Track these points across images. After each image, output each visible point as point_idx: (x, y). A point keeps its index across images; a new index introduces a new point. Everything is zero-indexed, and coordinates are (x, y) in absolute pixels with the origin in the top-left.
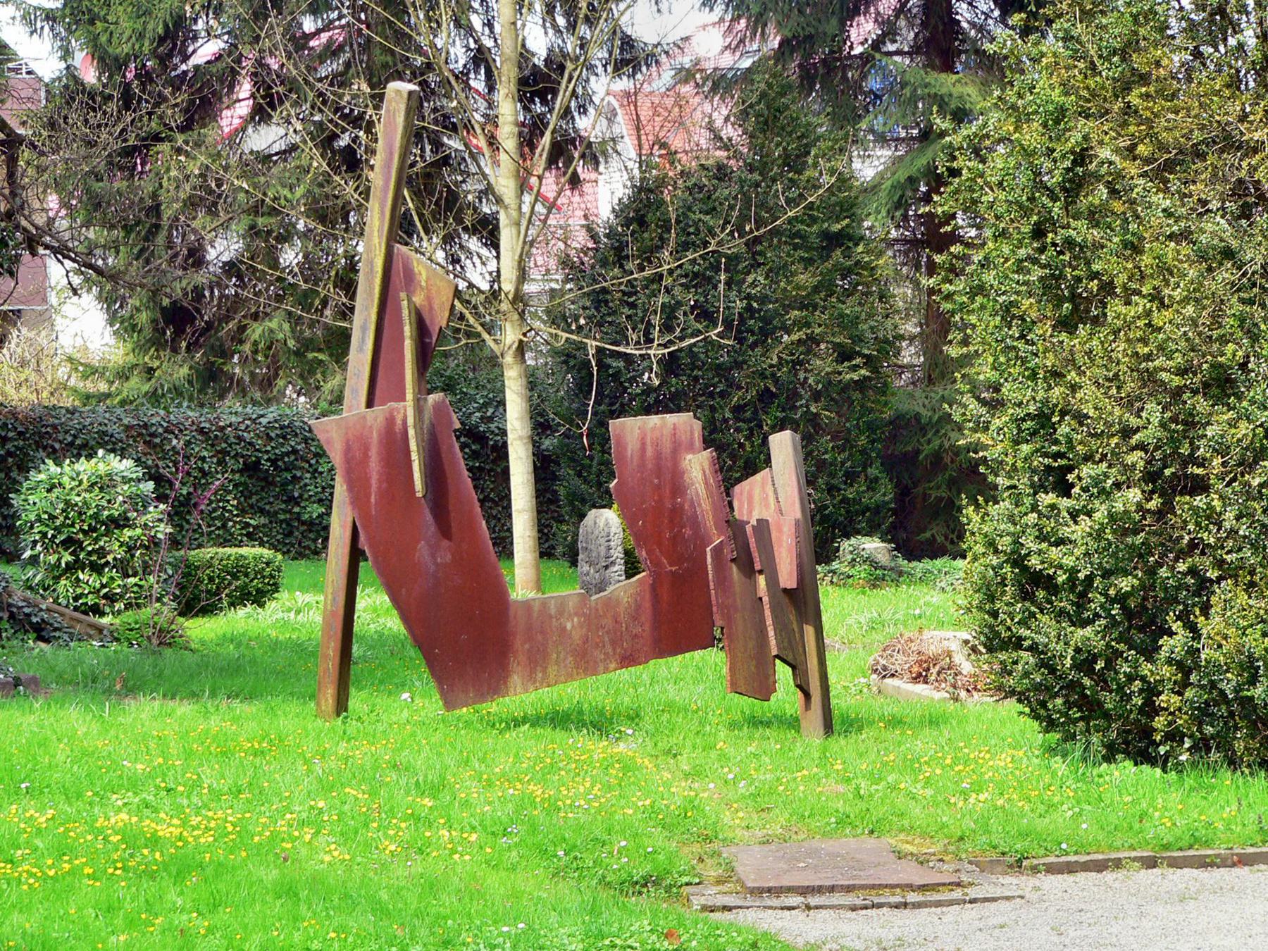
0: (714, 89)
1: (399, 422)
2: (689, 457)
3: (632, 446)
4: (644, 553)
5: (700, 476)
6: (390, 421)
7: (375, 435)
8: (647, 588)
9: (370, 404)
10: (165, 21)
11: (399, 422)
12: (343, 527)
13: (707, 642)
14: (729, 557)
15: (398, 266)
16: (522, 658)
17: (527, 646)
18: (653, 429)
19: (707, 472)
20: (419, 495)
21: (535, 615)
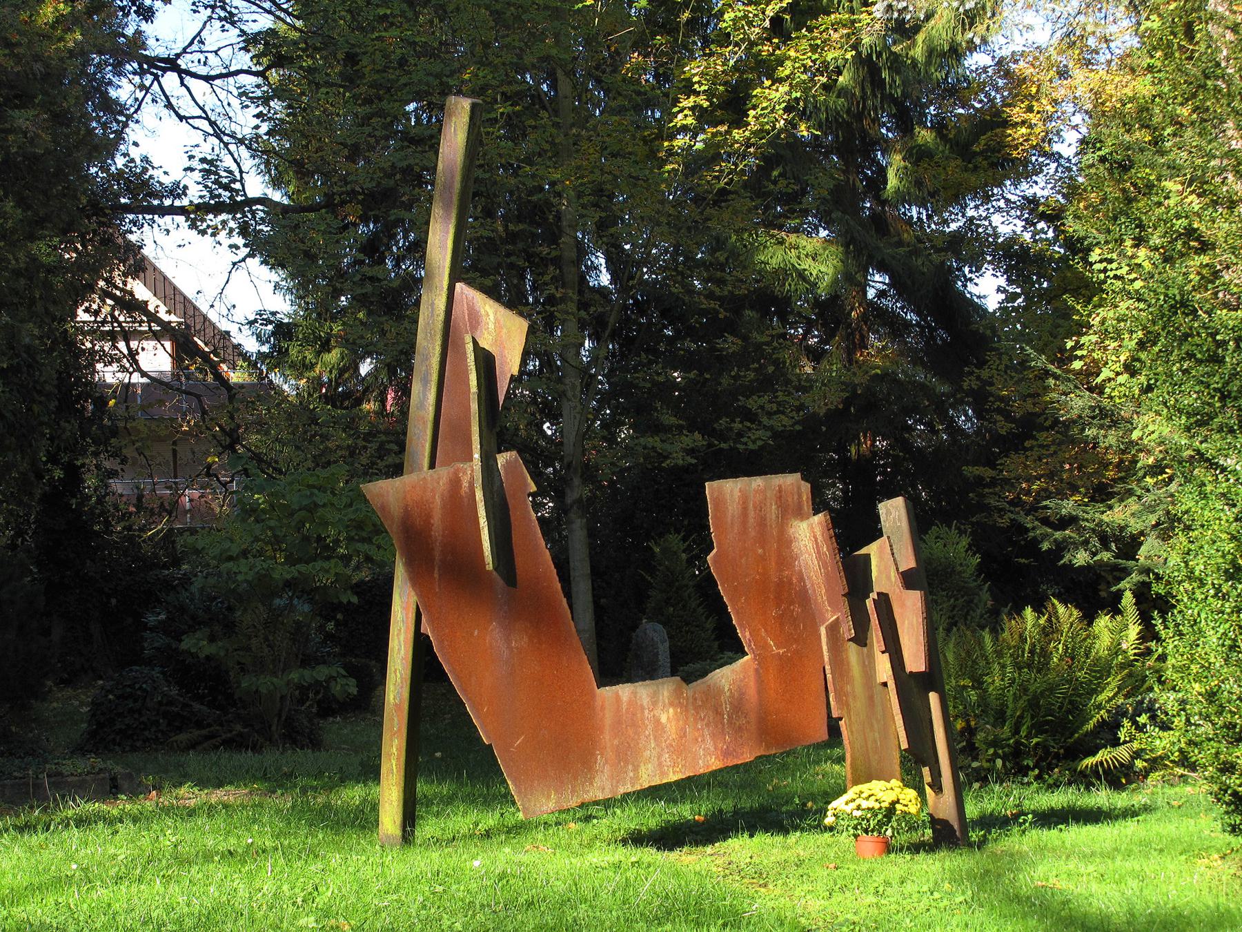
0: (639, 797)
1: (465, 484)
2: (796, 523)
3: (733, 508)
4: (747, 634)
5: (810, 546)
6: (455, 483)
7: (438, 500)
8: (751, 673)
9: (432, 465)
10: (637, 839)
11: (465, 484)
12: (405, 609)
13: (830, 735)
14: (847, 636)
15: (459, 310)
16: (610, 754)
17: (616, 742)
18: (756, 491)
19: (820, 539)
20: (490, 567)
21: (625, 706)
